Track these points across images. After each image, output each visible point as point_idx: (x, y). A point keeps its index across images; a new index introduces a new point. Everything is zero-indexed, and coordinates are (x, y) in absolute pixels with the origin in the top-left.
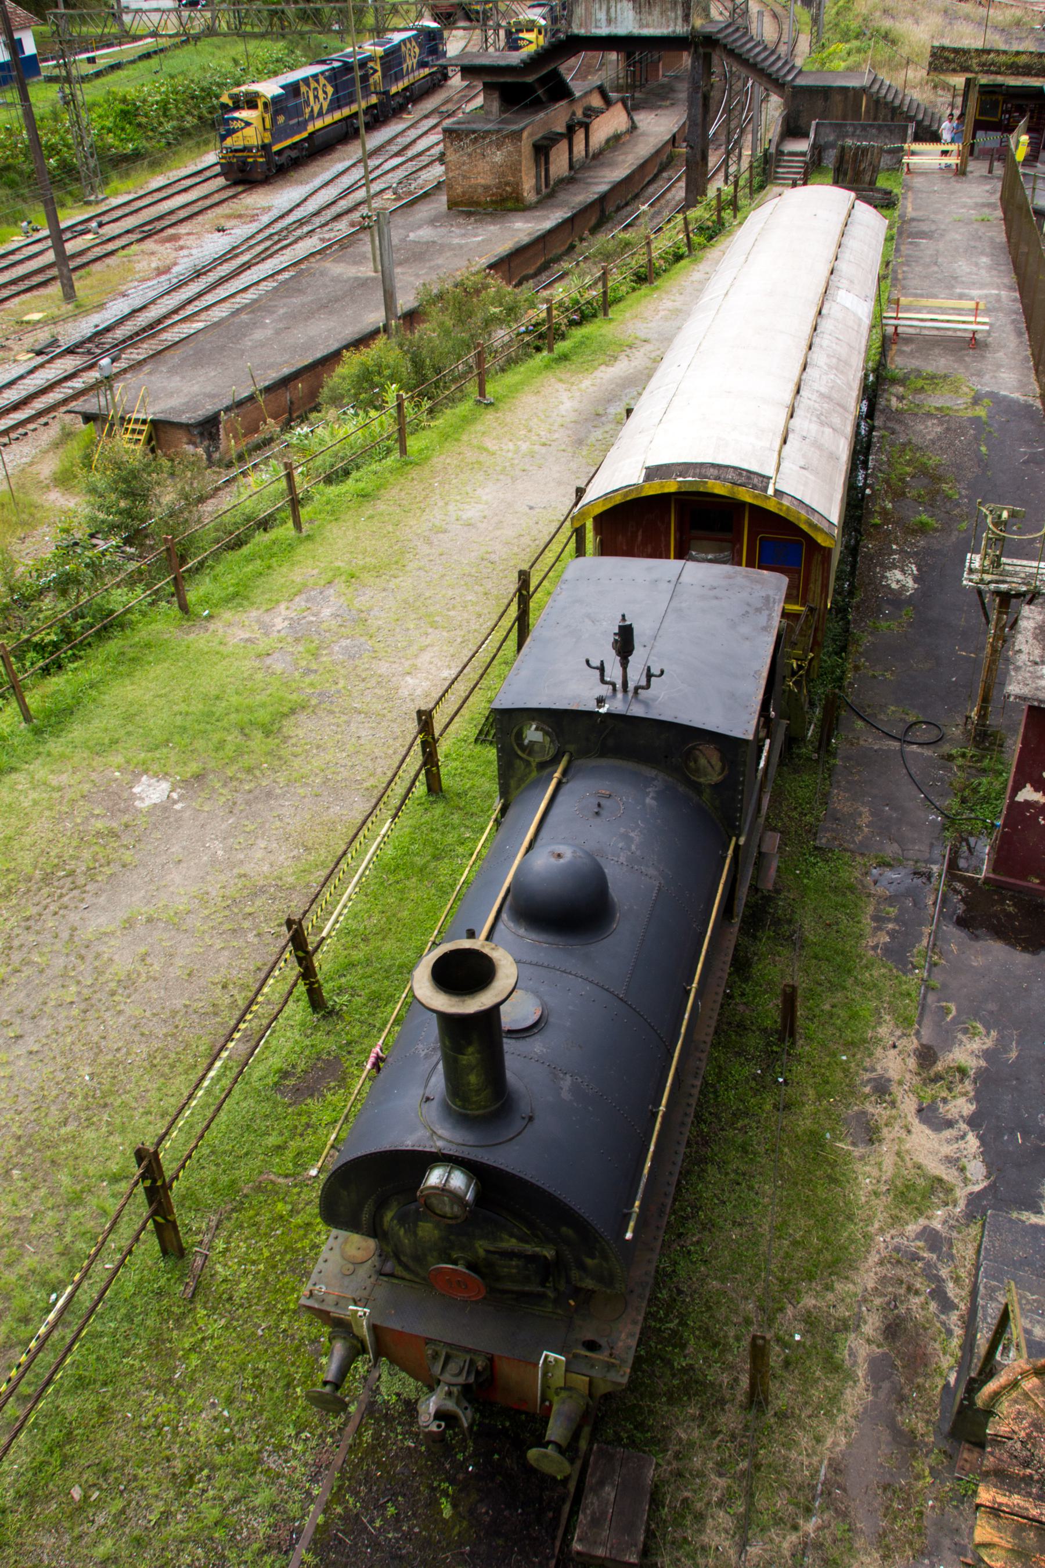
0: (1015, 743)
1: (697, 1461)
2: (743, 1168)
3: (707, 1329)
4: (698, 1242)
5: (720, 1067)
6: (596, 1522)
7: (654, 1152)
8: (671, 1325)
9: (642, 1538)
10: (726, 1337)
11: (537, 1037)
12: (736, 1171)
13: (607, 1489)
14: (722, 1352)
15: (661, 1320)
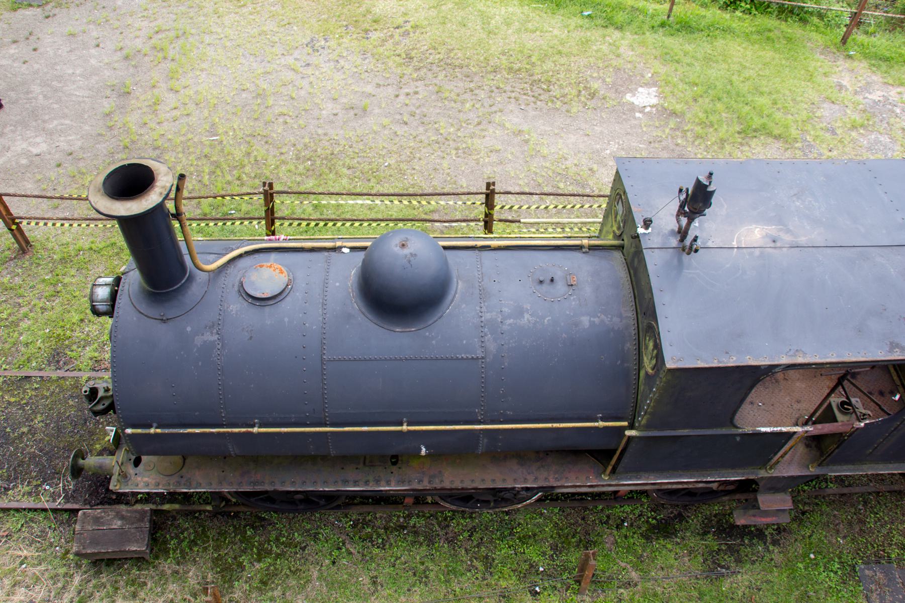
0: (231, 484)
1: (173, 587)
2: (432, 575)
3: (277, 575)
4: (350, 553)
5: (535, 535)
6: (97, 520)
7: (212, 433)
8: (274, 548)
9: (89, 551)
10: (272, 589)
11: (246, 304)
12: (427, 568)
13: (119, 523)
14: (260, 589)
15: (277, 539)
